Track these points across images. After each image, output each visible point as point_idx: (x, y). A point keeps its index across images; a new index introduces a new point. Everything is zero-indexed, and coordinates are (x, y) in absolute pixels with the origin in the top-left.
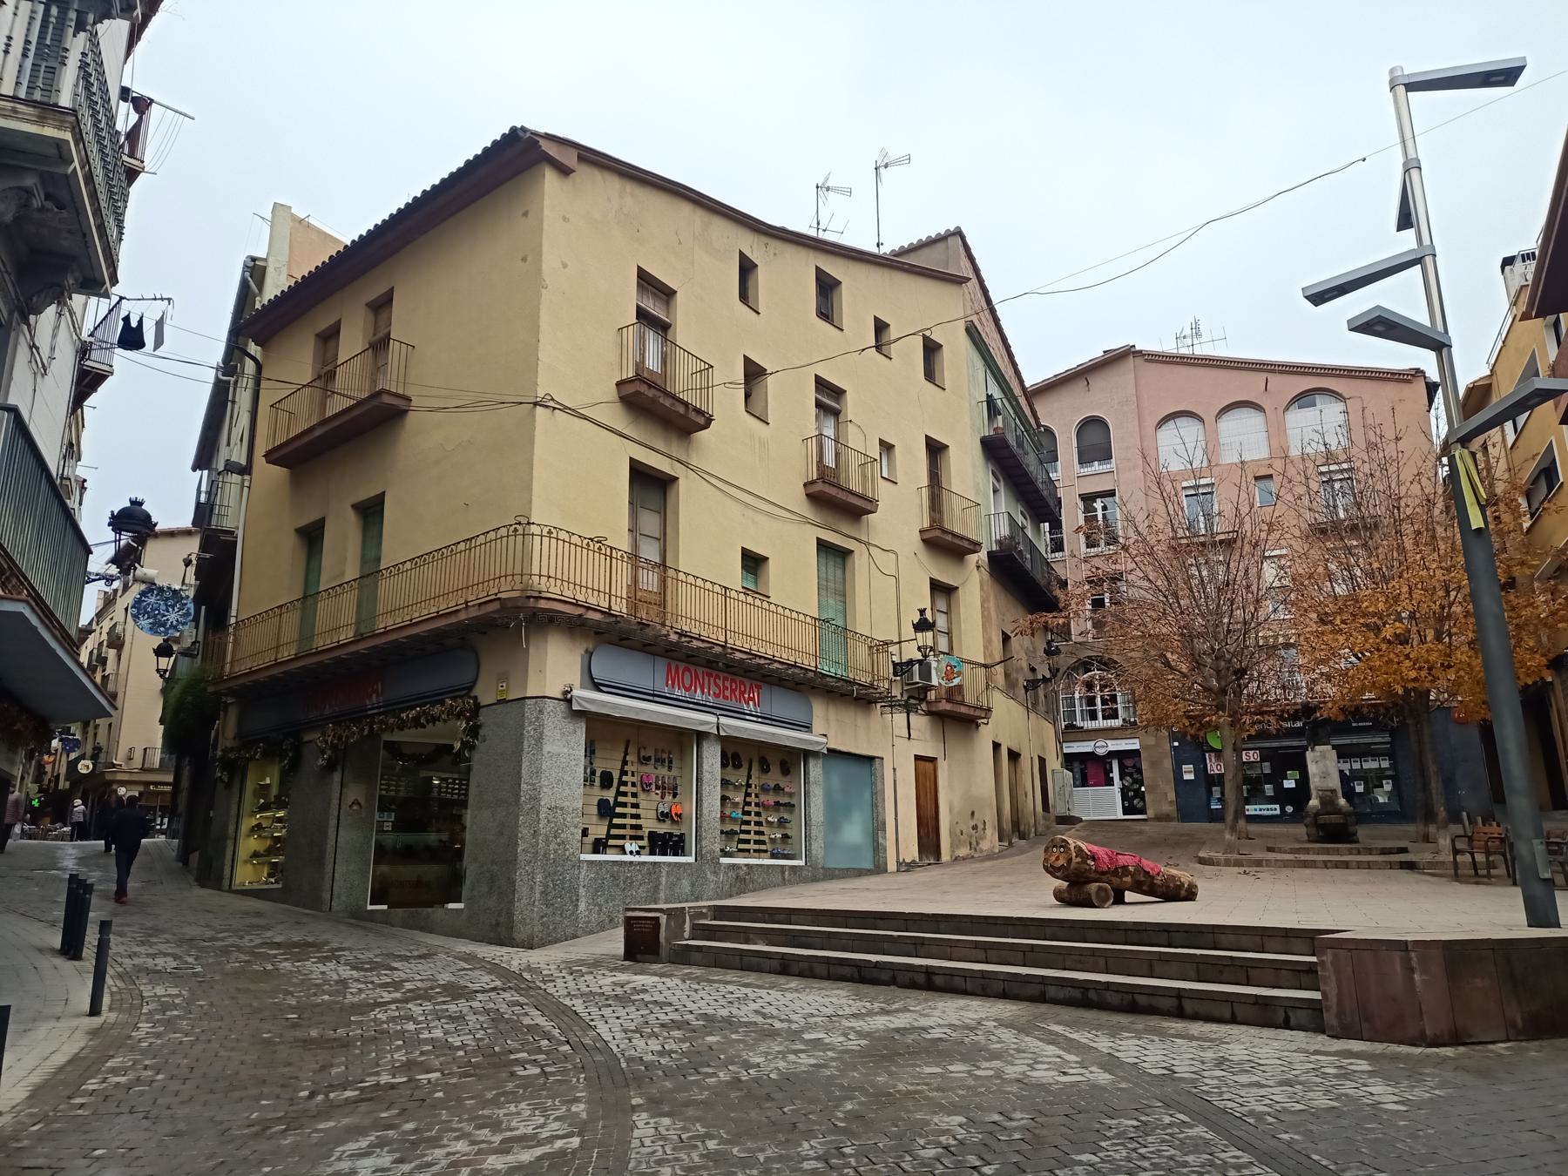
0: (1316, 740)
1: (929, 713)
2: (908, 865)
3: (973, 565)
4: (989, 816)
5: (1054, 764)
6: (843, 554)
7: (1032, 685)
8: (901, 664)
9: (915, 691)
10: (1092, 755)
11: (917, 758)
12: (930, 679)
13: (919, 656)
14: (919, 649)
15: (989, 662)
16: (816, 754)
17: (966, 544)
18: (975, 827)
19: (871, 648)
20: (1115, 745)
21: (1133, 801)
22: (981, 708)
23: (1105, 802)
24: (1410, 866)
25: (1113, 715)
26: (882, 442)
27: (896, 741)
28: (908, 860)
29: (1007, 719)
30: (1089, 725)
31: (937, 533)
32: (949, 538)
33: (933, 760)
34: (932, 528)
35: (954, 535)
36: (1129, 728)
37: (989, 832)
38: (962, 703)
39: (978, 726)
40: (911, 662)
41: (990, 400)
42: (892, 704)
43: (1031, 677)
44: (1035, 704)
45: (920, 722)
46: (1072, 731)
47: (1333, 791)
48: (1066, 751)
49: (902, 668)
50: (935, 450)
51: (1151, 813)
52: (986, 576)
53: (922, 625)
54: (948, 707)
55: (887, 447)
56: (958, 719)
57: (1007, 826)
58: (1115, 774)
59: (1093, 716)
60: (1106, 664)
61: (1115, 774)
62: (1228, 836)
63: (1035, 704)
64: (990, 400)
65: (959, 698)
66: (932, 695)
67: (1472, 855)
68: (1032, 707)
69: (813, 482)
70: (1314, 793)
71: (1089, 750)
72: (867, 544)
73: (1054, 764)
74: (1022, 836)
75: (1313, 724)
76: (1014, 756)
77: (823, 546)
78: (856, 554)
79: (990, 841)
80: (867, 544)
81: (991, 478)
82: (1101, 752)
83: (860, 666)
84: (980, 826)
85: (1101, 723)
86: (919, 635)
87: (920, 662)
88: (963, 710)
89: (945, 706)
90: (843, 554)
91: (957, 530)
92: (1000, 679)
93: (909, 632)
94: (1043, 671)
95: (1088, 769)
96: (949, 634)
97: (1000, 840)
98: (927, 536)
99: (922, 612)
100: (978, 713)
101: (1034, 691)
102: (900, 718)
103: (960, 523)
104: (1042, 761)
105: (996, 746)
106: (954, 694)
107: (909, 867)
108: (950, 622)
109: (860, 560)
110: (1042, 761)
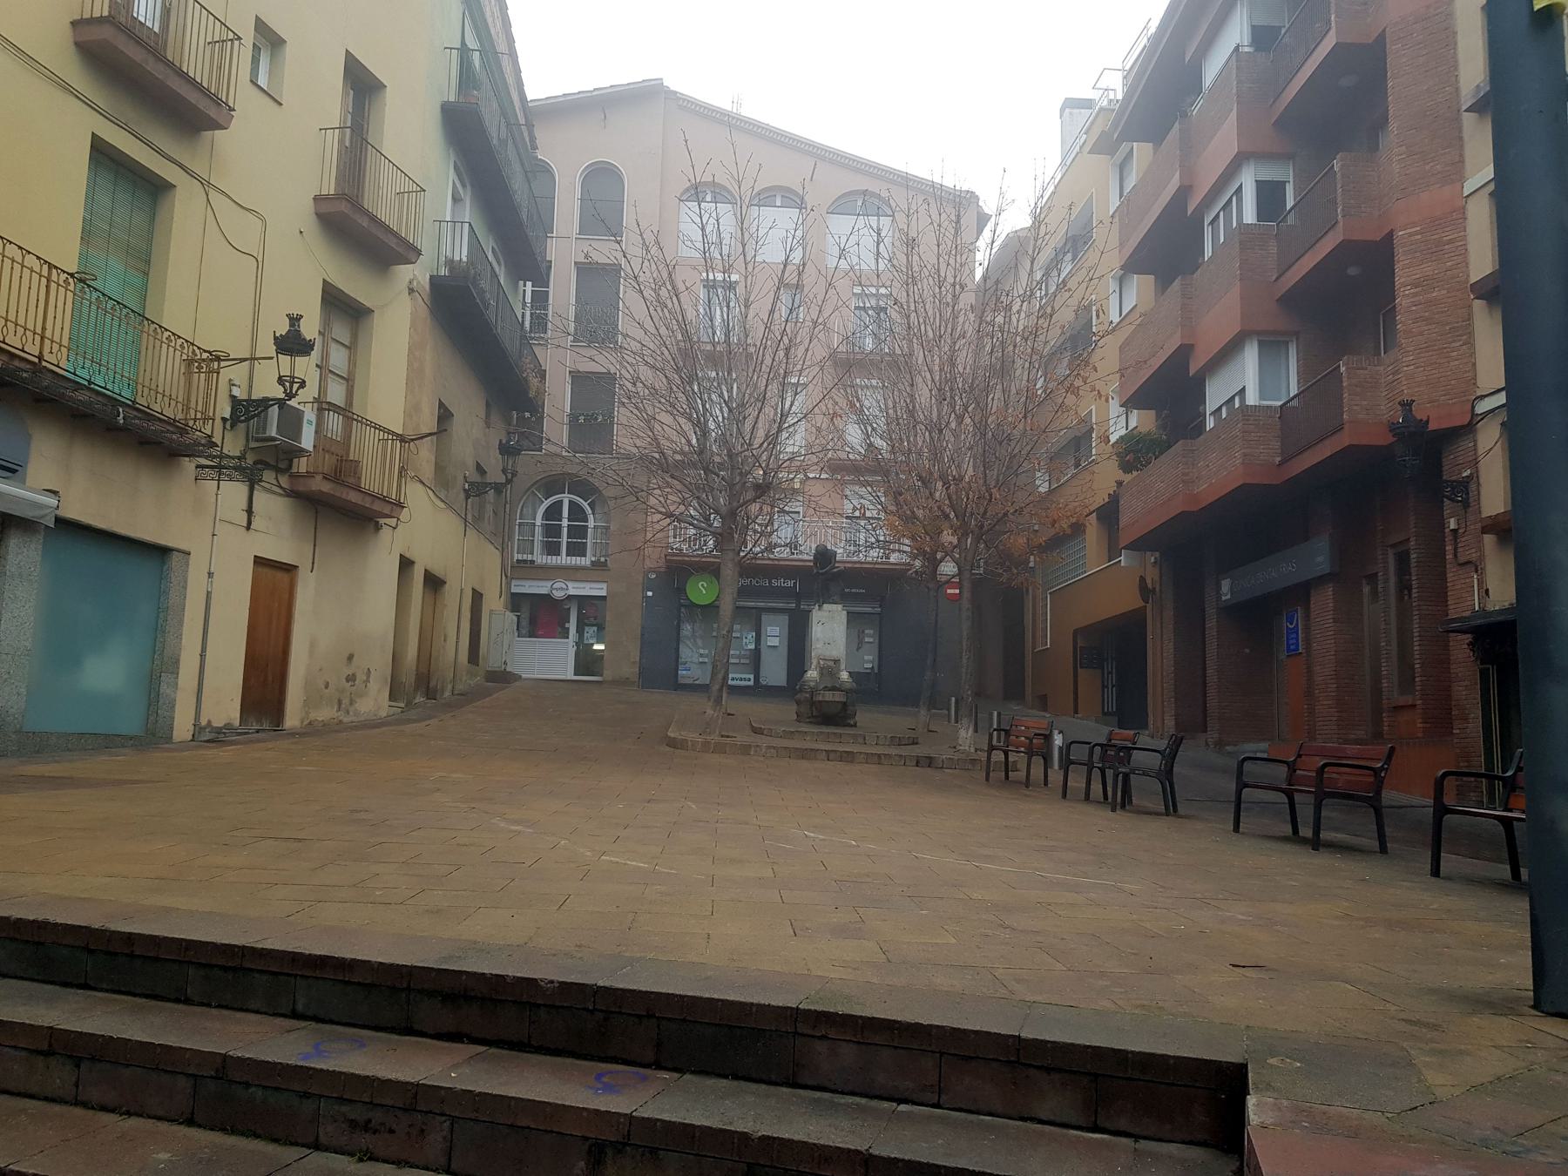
0: (824, 598)
1: (292, 494)
2: (219, 731)
3: (403, 286)
4: (379, 663)
5: (494, 602)
6: (153, 189)
7: (475, 490)
8: (249, 401)
9: (264, 449)
10: (547, 598)
11: (259, 561)
12: (297, 435)
13: (279, 393)
14: (281, 380)
15: (410, 433)
16: (26, 525)
17: (393, 242)
18: (351, 678)
19: (189, 362)
20: (575, 589)
21: (587, 662)
22: (384, 499)
23: (550, 659)
24: (930, 762)
25: (577, 549)
26: (261, 26)
27: (220, 534)
28: (218, 723)
29: (426, 528)
30: (540, 558)
31: (343, 207)
32: (365, 223)
33: (290, 569)
34: (340, 197)
35: (373, 219)
36: (599, 568)
37: (374, 686)
38: (358, 489)
39: (378, 527)
40: (265, 403)
41: (464, 50)
42: (221, 468)
43: (476, 478)
44: (478, 519)
45: (270, 504)
46: (526, 569)
47: (836, 661)
48: (514, 590)
49: (247, 411)
50: (362, 85)
51: (608, 674)
52: (424, 311)
53: (291, 344)
54: (326, 487)
55: (269, 40)
56: (341, 508)
57: (408, 677)
58: (572, 626)
59: (552, 549)
60: (582, 487)
61: (572, 626)
62: (710, 712)
63: (478, 519)
64: (464, 50)
65: (351, 480)
66: (302, 465)
67: (1006, 754)
68: (473, 521)
69: (92, 21)
70: (815, 662)
71: (544, 591)
72: (205, 184)
73: (494, 602)
74: (431, 694)
75: (823, 578)
76: (434, 583)
77: (101, 153)
78: (180, 195)
79: (375, 701)
80: (205, 184)
81: (452, 174)
82: (558, 594)
83: (160, 385)
84: (361, 677)
85: (564, 559)
86: (285, 360)
87: (281, 403)
88: (353, 497)
89: (319, 485)
90: (153, 189)
91: (383, 215)
92: (427, 468)
93: (267, 347)
94: (495, 476)
95: (542, 617)
96: (349, 380)
97: (392, 697)
98: (326, 208)
99: (294, 320)
100: (377, 506)
101: (480, 498)
102: (233, 493)
103: (383, 201)
104: (477, 597)
105: (406, 564)
106: (344, 471)
107: (218, 737)
108: (352, 362)
109: (185, 207)
110: (477, 597)
